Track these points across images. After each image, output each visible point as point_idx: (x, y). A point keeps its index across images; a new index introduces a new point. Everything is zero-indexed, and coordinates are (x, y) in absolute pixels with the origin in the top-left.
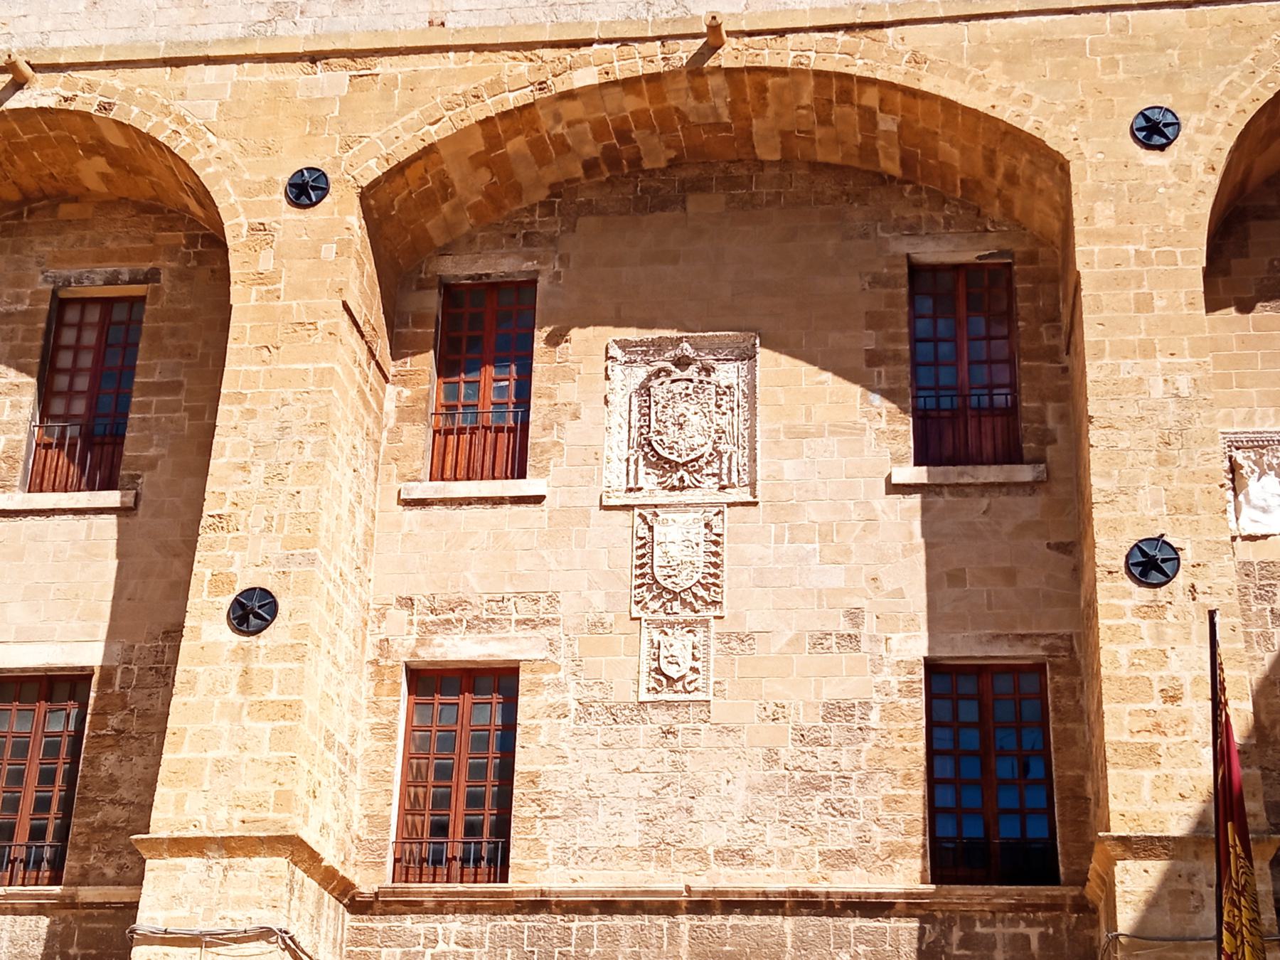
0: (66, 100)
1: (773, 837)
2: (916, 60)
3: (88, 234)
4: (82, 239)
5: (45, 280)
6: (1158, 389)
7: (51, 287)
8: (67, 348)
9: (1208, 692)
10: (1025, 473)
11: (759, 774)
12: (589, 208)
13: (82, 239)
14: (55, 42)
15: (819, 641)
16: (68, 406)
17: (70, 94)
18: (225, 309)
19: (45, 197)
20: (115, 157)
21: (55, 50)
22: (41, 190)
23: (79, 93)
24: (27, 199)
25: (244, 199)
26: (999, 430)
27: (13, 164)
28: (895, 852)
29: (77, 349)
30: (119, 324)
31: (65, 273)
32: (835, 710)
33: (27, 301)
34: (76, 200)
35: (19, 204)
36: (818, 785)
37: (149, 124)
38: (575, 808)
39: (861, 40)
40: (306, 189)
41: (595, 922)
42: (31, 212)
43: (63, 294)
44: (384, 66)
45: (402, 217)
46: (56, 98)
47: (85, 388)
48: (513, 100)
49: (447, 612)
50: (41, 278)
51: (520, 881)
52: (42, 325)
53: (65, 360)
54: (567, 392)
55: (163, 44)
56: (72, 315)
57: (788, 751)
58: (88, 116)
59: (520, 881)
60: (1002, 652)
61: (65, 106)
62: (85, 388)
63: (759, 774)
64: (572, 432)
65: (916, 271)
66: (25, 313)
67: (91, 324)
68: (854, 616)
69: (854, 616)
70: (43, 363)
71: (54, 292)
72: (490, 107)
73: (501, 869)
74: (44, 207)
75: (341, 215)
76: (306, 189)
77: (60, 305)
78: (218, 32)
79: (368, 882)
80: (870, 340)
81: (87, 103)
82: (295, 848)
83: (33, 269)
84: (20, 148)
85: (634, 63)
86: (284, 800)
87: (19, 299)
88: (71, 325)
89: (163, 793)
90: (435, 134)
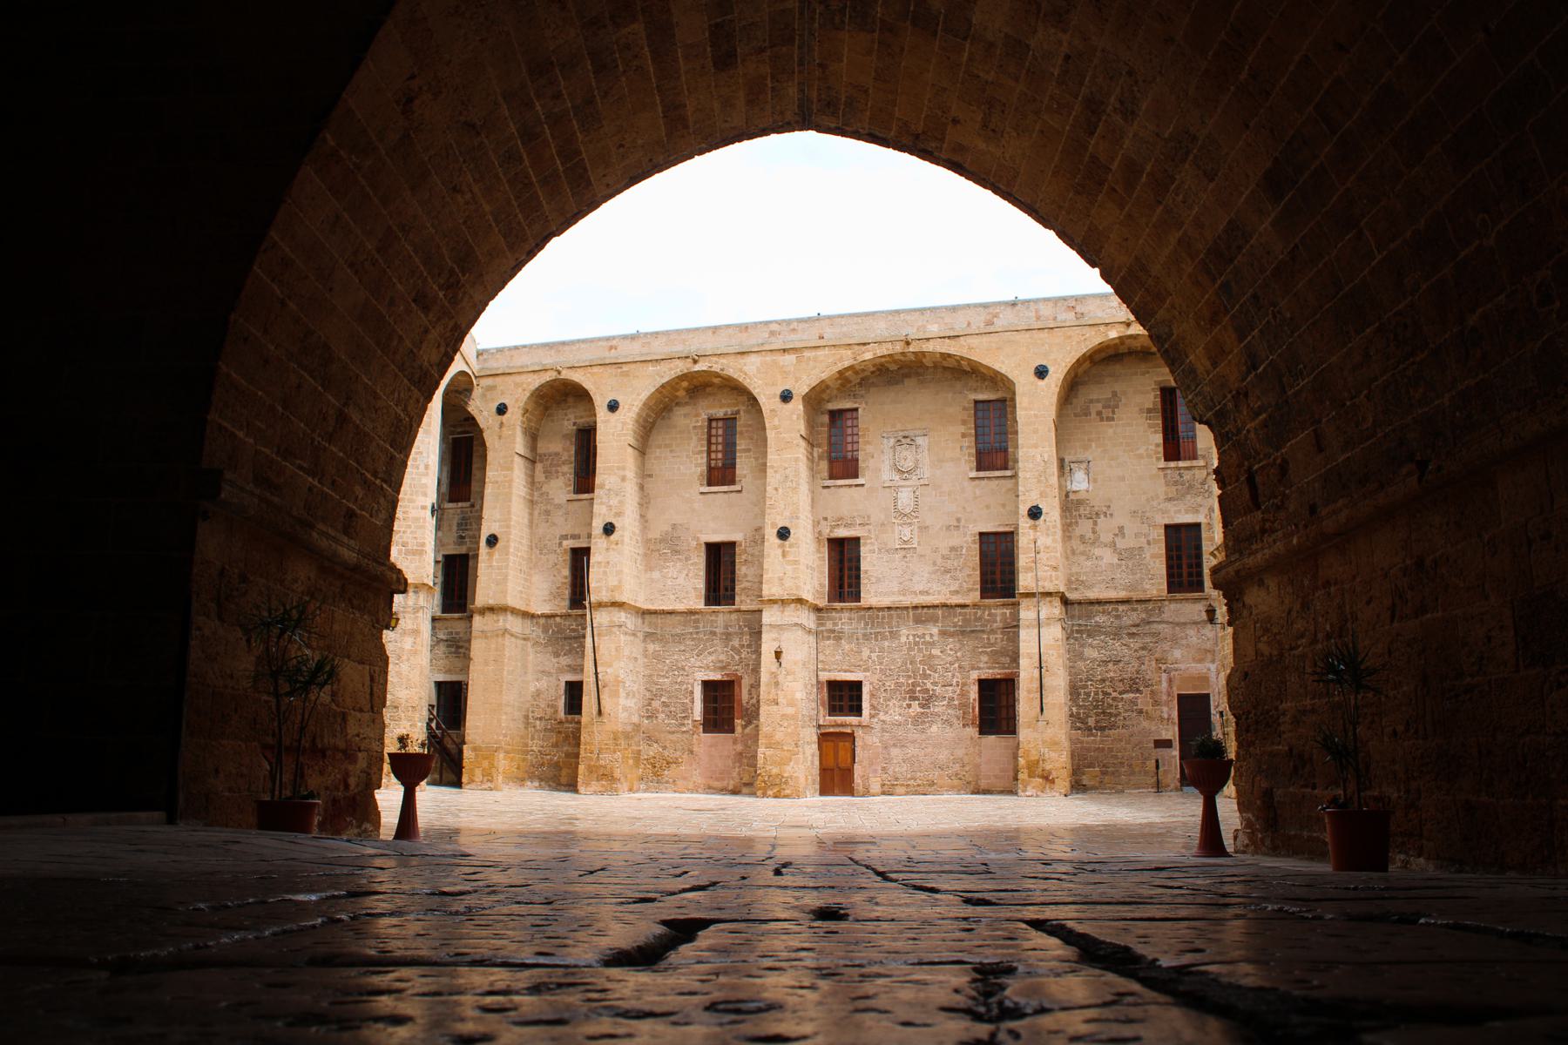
1: (935, 587)
2: (970, 348)
6: (1039, 458)
10: (1008, 473)
11: (931, 568)
12: (873, 385)
15: (948, 528)
18: (765, 440)
25: (767, 399)
28: (970, 590)
30: (730, 422)
32: (953, 549)
36: (948, 571)
38: (878, 580)
39: (952, 342)
40: (786, 397)
41: (886, 613)
44: (806, 354)
45: (815, 399)
48: (847, 364)
49: (839, 521)
51: (863, 603)
53: (713, 440)
54: (870, 449)
57: (939, 561)
59: (863, 603)
60: (1001, 529)
63: (931, 568)
64: (872, 463)
65: (976, 402)
68: (958, 520)
69: (958, 520)
72: (840, 367)
73: (858, 598)
75: (797, 406)
76: (786, 397)
77: (710, 420)
78: (754, 342)
79: (823, 603)
80: (962, 429)
81: (716, 368)
82: (800, 601)
85: (883, 350)
86: (798, 588)
89: (764, 586)
90: (824, 376)
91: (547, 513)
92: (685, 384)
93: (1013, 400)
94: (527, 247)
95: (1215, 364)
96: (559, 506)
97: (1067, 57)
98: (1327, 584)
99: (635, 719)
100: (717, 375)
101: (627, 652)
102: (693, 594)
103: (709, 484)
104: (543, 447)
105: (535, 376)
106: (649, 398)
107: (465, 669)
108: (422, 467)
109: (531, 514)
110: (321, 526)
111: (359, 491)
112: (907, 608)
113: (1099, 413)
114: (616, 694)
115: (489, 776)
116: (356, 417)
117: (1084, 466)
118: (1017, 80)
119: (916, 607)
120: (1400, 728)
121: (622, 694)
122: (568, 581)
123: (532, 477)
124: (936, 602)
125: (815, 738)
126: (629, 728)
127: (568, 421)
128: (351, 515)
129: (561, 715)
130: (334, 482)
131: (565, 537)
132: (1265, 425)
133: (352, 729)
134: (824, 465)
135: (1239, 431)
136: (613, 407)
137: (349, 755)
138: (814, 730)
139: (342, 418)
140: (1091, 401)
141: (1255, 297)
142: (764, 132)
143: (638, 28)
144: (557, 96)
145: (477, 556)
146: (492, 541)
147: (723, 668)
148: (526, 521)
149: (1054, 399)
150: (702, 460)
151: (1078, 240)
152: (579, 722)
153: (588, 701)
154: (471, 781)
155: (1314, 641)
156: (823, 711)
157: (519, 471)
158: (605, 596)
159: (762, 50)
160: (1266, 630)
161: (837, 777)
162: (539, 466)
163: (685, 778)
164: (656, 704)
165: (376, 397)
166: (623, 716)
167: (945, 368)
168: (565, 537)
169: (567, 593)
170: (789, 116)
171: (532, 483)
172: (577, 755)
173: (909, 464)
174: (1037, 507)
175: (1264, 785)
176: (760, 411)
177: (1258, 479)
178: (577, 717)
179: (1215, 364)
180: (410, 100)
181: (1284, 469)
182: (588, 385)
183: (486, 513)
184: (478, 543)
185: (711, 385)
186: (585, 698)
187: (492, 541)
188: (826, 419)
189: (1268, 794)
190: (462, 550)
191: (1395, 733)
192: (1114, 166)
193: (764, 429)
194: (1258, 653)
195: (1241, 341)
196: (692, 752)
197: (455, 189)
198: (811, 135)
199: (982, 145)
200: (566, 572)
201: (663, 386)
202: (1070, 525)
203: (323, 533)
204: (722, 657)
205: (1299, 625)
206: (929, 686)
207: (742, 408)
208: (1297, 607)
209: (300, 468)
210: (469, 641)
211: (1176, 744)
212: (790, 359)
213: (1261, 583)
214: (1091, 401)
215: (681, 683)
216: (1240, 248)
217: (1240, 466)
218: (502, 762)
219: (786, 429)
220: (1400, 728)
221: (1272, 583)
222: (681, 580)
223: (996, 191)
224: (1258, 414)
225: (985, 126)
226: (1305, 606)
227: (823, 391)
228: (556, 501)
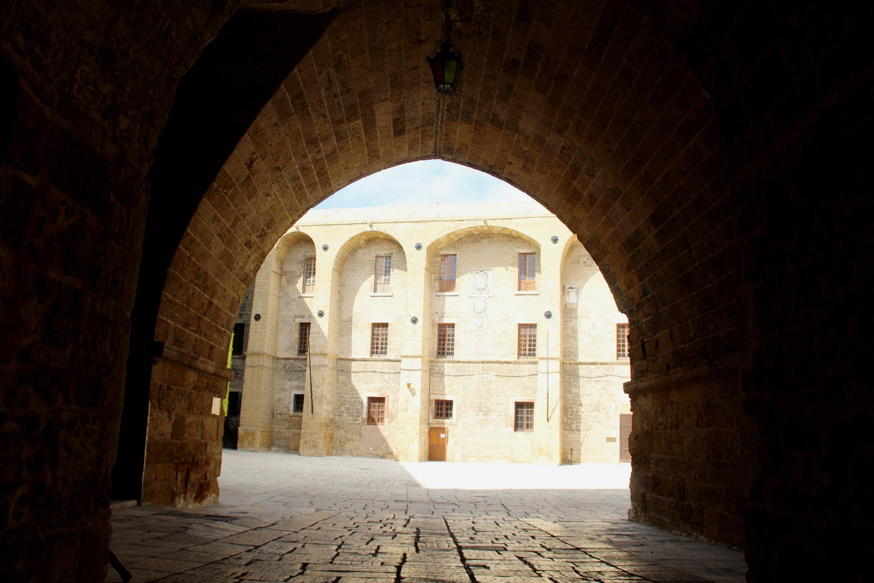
12: (465, 242)
48: (451, 231)
72: (448, 232)
75: (423, 252)
77: (377, 257)
81: (381, 230)
91: (288, 303)
92: (364, 237)
93: (539, 253)
94: (299, 214)
95: (629, 289)
96: (294, 300)
97: (563, 148)
98: (672, 403)
99: (331, 416)
100: (382, 233)
101: (328, 380)
104: (286, 267)
107: (241, 385)
109: (279, 304)
110: (201, 359)
111: (216, 336)
112: (478, 363)
113: (585, 262)
114: (321, 403)
115: (251, 444)
116: (216, 301)
117: (574, 290)
118: (540, 152)
119: (483, 362)
120: (697, 476)
121: (325, 402)
122: (298, 340)
123: (280, 283)
124: (494, 360)
125: (427, 430)
126: (328, 421)
127: (301, 253)
128: (212, 347)
129: (292, 412)
130: (205, 334)
131: (296, 317)
132: (649, 322)
133: (209, 451)
134: (437, 284)
135: (639, 322)
136: (325, 248)
137: (207, 463)
138: (426, 426)
139: (210, 303)
140: (581, 256)
141: (646, 264)
142: (417, 159)
143: (360, 122)
144: (319, 151)
145: (249, 325)
146: (258, 317)
147: (380, 390)
149: (561, 255)
151: (567, 221)
152: (301, 417)
153: (306, 405)
154: (242, 447)
155: (666, 428)
156: (432, 416)
157: (273, 281)
158: (317, 350)
159: (417, 128)
160: (646, 418)
161: (435, 452)
162: (284, 278)
163: (356, 449)
164: (342, 408)
165: (225, 290)
166: (325, 414)
167: (504, 235)
168: (296, 317)
169: (297, 347)
170: (429, 153)
171: (281, 287)
172: (299, 435)
173: (482, 286)
174: (549, 312)
175: (643, 491)
176: (404, 253)
177: (646, 346)
178: (300, 414)
179: (629, 289)
180: (252, 162)
181: (657, 344)
183: (255, 303)
184: (250, 318)
186: (305, 405)
187: (258, 317)
188: (439, 259)
189: (644, 495)
190: (241, 321)
191: (695, 478)
192: (585, 194)
193: (406, 263)
194: (642, 427)
195: (641, 281)
196: (361, 435)
197: (268, 195)
198: (439, 162)
199: (522, 175)
200: (297, 335)
202: (567, 321)
203: (203, 362)
204: (379, 385)
205: (660, 419)
206: (489, 404)
207: (394, 252)
208: (659, 410)
209: (192, 331)
210: (243, 371)
211: (618, 440)
212: (421, 226)
213: (645, 395)
214: (581, 256)
216: (640, 242)
217: (639, 337)
218: (259, 437)
219: (417, 261)
220: (697, 476)
221: (650, 396)
223: (529, 193)
224: (647, 316)
225: (524, 167)
226: (663, 411)
227: (438, 245)
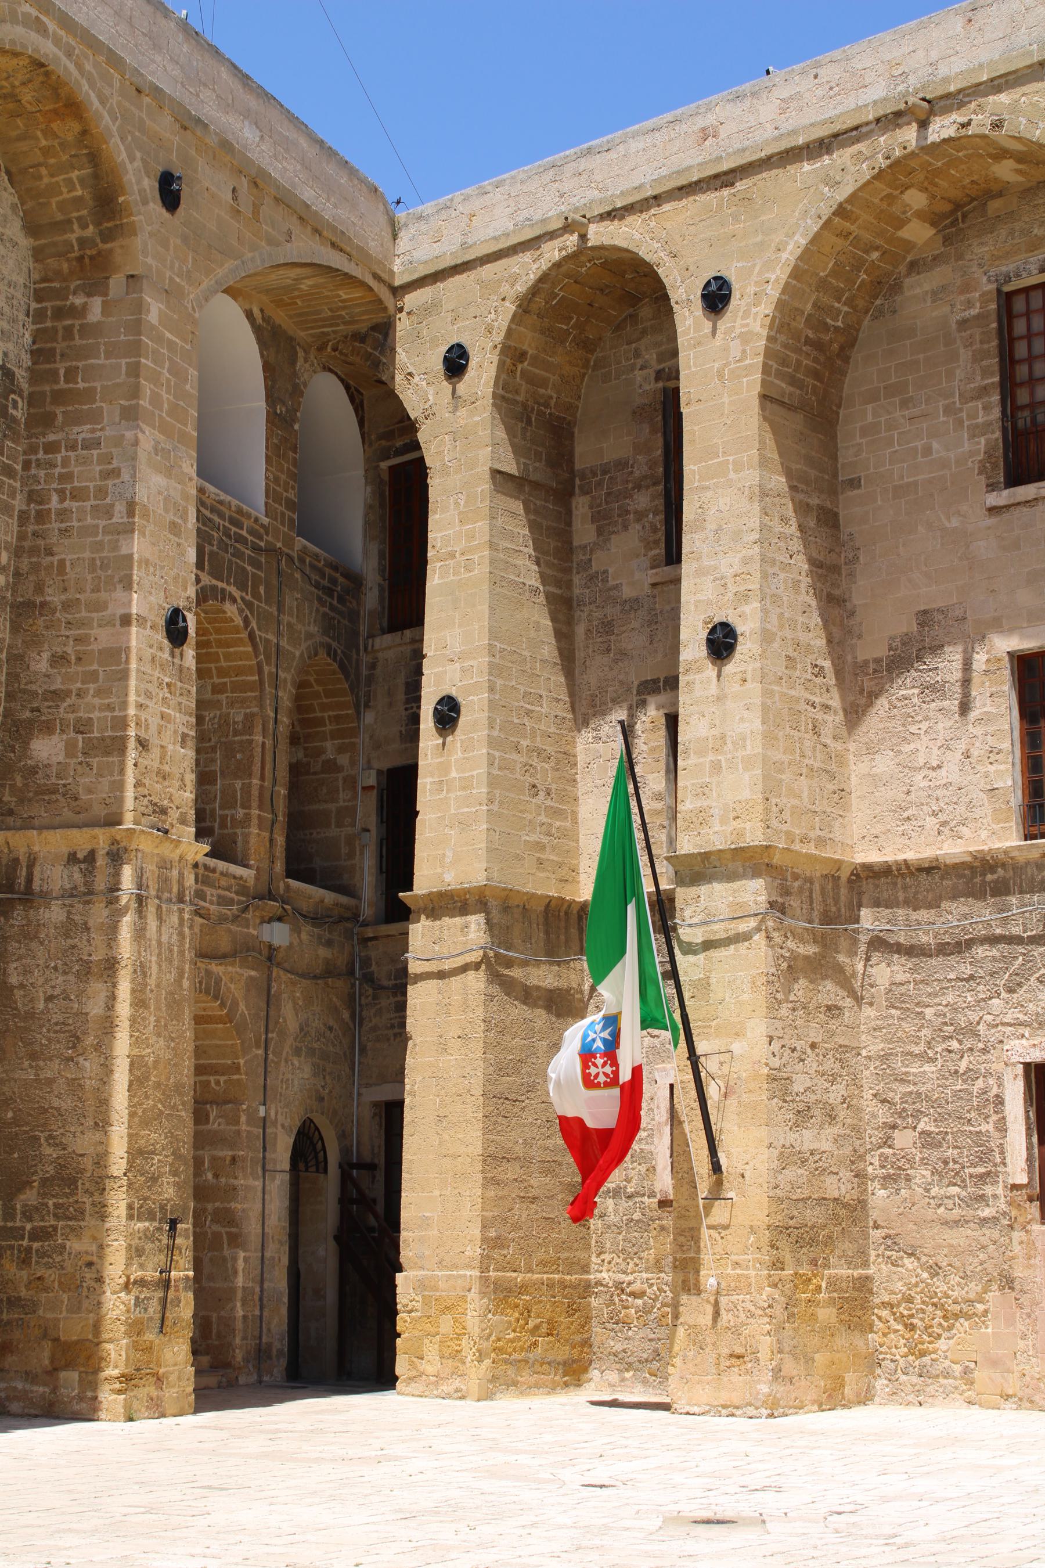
0: (963, 126)
3: (1017, 226)
4: (1012, 232)
5: (989, 281)
7: (994, 286)
8: (1021, 338)
9: (680, 748)
13: (1012, 232)
14: (943, 71)
16: (1032, 394)
17: (965, 120)
19: (973, 200)
20: (1020, 158)
21: (946, 80)
22: (968, 195)
23: (973, 116)
24: (958, 206)
26: (645, 871)
27: (936, 185)
29: (1029, 336)
31: (1004, 269)
33: (978, 305)
34: (1000, 194)
35: (953, 212)
37: (1038, 132)
42: (964, 216)
43: (1007, 289)
46: (955, 127)
47: (1042, 351)
50: (985, 279)
52: (994, 325)
55: (1035, 46)
56: (1019, 305)
58: (984, 137)
61: (963, 132)
62: (1042, 328)
66: (978, 317)
67: (1037, 311)
70: (1002, 360)
71: (999, 291)
74: (975, 208)
77: (1006, 299)
81: (980, 121)
83: (978, 273)
84: (937, 172)
87: (969, 304)
88: (1021, 338)
91: (607, 627)
92: (916, 199)
96: (634, 604)
102: (985, 810)
103: (1014, 480)
105: (526, 257)
106: (806, 255)
108: (120, 508)
148: (549, 650)
150: (988, 413)
163: (994, 1363)
182: (649, 251)
185: (993, 191)
201: (841, 211)
215: (971, 1076)
222: (951, 773)
228: (627, 592)
